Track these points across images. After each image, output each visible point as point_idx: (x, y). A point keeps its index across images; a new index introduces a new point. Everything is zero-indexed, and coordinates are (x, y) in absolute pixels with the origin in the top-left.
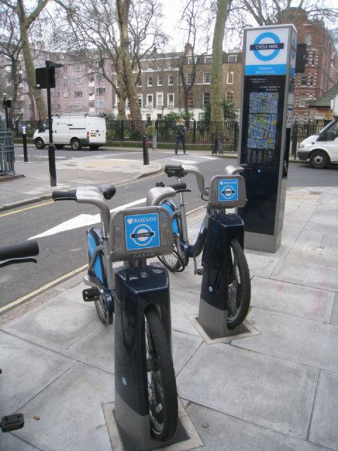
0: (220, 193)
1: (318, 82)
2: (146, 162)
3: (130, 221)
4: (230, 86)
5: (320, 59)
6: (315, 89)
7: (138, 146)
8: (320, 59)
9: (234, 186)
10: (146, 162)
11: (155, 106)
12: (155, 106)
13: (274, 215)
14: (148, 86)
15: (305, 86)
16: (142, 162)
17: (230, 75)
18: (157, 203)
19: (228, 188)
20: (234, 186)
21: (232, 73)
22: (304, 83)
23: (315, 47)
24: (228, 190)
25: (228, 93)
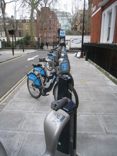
0: (62, 68)
1: (54, 29)
2: (24, 52)
3: (63, 65)
4: (27, 30)
5: (54, 22)
6: (54, 31)
7: (11, 49)
8: (54, 22)
9: (66, 65)
10: (24, 52)
11: (2, 36)
12: (2, 36)
13: (63, 129)
14: (3, 29)
15: (50, 30)
16: (23, 52)
17: (27, 26)
18: (63, 61)
19: (65, 66)
20: (66, 65)
21: (28, 26)
22: (50, 29)
23: (53, 19)
24: (65, 67)
25: (27, 32)
